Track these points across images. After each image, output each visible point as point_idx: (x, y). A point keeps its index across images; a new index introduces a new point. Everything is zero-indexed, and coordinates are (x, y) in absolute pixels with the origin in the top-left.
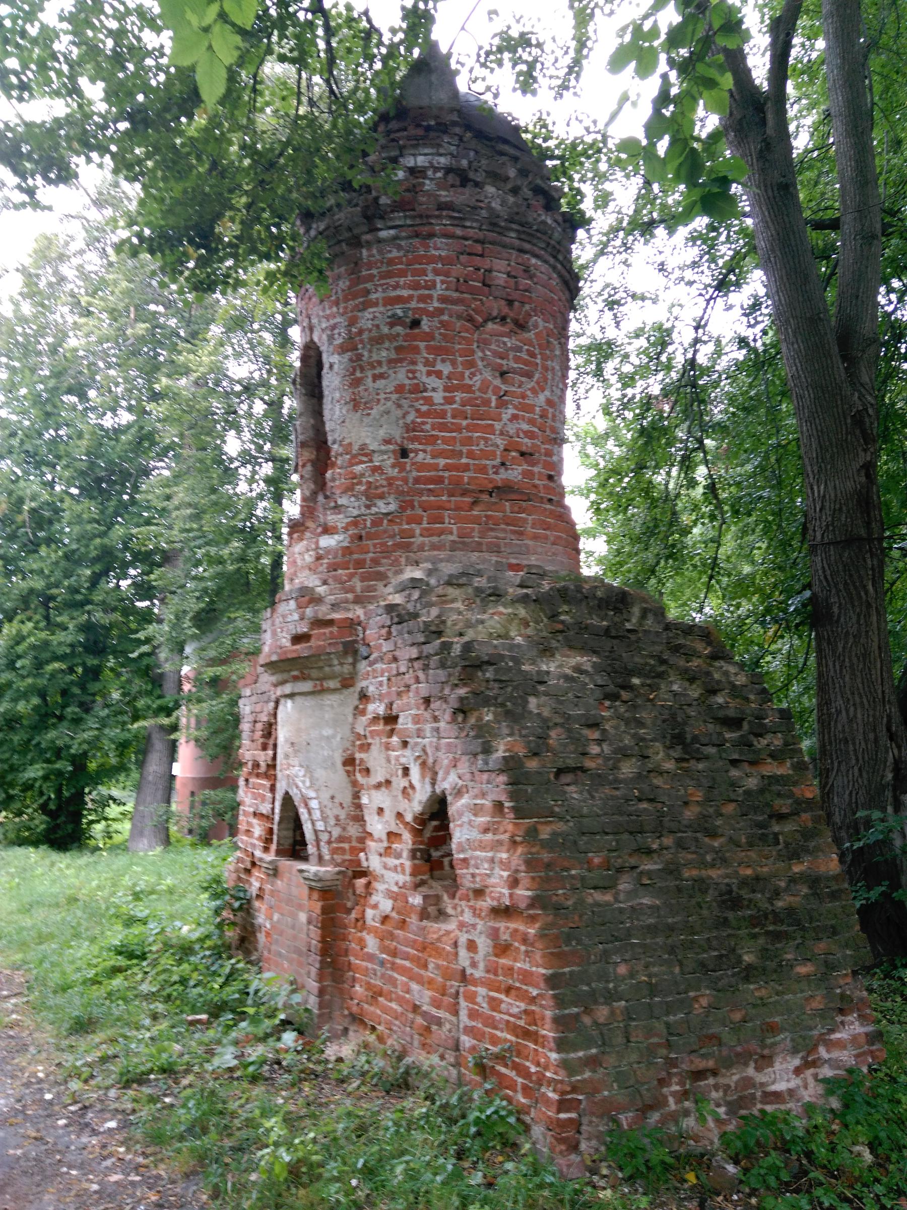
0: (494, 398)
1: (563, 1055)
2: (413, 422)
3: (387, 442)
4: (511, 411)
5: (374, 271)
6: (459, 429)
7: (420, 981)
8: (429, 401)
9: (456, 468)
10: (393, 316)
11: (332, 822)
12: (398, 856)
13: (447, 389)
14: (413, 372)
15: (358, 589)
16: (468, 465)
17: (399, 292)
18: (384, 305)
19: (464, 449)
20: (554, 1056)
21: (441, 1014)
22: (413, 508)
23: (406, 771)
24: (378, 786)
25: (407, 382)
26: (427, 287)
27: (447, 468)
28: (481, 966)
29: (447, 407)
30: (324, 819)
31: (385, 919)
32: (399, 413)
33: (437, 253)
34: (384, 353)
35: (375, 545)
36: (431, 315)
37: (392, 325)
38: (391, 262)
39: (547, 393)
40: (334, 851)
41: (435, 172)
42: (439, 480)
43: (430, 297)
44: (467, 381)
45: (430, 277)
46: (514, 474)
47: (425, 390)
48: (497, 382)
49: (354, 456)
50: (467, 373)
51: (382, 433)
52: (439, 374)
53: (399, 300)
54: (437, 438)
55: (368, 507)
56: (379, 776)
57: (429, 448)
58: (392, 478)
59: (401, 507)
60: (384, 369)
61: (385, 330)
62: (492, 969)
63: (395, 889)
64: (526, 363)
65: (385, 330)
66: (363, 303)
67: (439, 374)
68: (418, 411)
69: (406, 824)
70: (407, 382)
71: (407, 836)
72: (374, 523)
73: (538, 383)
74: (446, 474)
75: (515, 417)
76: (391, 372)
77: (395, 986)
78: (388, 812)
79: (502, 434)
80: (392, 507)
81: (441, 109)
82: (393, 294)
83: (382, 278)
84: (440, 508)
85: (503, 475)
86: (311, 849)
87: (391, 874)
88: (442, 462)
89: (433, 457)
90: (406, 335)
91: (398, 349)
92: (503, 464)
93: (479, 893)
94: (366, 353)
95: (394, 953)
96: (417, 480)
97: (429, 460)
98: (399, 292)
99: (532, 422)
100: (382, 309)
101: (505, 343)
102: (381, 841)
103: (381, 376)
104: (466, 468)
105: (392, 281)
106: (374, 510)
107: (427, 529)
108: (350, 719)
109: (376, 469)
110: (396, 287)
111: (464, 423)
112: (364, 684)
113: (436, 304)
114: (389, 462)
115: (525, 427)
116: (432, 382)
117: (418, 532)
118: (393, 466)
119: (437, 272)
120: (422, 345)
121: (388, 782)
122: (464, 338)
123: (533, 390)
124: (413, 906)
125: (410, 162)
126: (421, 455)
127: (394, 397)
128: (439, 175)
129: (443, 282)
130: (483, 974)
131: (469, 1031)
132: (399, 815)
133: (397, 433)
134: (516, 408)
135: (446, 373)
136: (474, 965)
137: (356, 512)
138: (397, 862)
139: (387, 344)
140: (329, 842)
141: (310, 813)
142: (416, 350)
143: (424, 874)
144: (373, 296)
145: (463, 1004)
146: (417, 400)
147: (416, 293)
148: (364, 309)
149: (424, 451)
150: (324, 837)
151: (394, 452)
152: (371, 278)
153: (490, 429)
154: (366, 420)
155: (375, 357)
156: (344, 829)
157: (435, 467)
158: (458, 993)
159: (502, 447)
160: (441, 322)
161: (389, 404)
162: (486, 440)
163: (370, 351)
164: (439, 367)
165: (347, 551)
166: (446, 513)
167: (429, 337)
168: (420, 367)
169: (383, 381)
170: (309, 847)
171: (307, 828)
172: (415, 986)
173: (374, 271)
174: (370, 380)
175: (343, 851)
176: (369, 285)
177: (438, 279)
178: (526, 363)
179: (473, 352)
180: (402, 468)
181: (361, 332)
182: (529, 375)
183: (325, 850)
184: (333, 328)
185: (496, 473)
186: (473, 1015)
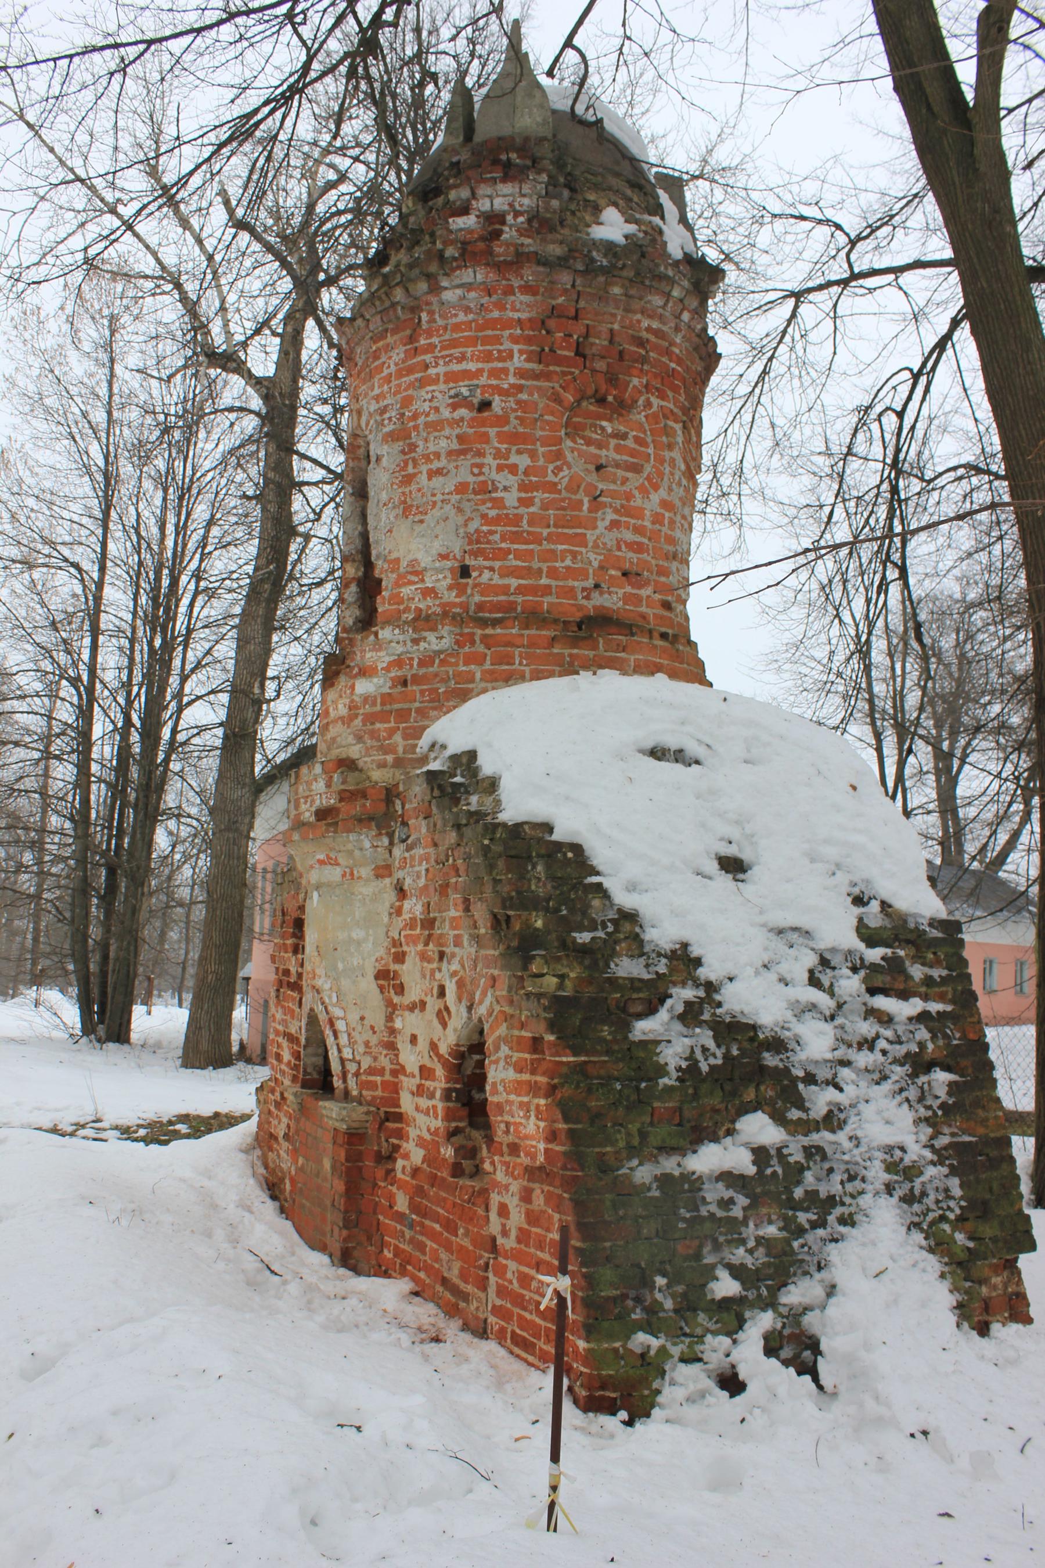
0: (586, 500)
1: (592, 1345)
2: (477, 531)
3: (444, 557)
4: (610, 516)
5: (435, 340)
6: (537, 540)
7: (448, 1247)
8: (499, 503)
9: (533, 590)
10: (456, 395)
11: (361, 1049)
12: (431, 1096)
13: (523, 487)
14: (480, 466)
15: (400, 749)
16: (549, 587)
17: (464, 366)
18: (445, 382)
19: (544, 567)
20: (582, 1344)
21: (469, 1288)
22: (473, 643)
23: (442, 993)
24: (412, 1008)
25: (471, 479)
26: (500, 359)
27: (521, 590)
28: (513, 1234)
29: (522, 510)
30: (352, 1043)
31: (416, 1171)
32: (460, 520)
33: (516, 315)
34: (443, 443)
35: (422, 692)
36: (504, 393)
37: (454, 407)
38: (457, 327)
39: (662, 493)
40: (363, 1085)
41: (515, 217)
42: (511, 607)
43: (505, 371)
44: (551, 477)
45: (507, 345)
46: (612, 600)
47: (496, 489)
48: (592, 478)
49: (401, 577)
50: (551, 467)
51: (437, 547)
52: (513, 469)
53: (467, 374)
54: (509, 551)
55: (416, 642)
56: (413, 994)
57: (497, 564)
58: (448, 604)
59: (457, 642)
60: (443, 463)
61: (446, 413)
62: (523, 1236)
63: (427, 1137)
64: (633, 453)
65: (446, 413)
66: (420, 380)
67: (513, 469)
68: (484, 516)
69: (440, 1056)
70: (471, 479)
71: (440, 1072)
72: (422, 663)
73: (648, 478)
74: (520, 599)
75: (614, 524)
76: (451, 466)
77: (424, 1253)
78: (425, 1040)
79: (596, 546)
80: (446, 643)
81: (527, 139)
82: (455, 367)
83: (443, 348)
84: (508, 644)
85: (598, 600)
86: (337, 1083)
87: (424, 1117)
88: (514, 583)
89: (501, 576)
90: (473, 419)
91: (461, 438)
92: (597, 586)
93: (514, 1149)
94: (421, 443)
95: (424, 1213)
96: (480, 607)
97: (497, 580)
98: (464, 366)
99: (638, 530)
100: (442, 387)
101: (603, 429)
102: (414, 1076)
103: (439, 472)
104: (547, 590)
105: (456, 352)
106: (423, 645)
107: (492, 672)
108: (386, 919)
109: (427, 592)
110: (462, 358)
111: (545, 532)
112: (400, 874)
113: (512, 380)
114: (445, 583)
115: (629, 536)
116: (505, 479)
117: (478, 676)
118: (450, 588)
119: (515, 340)
120: (492, 432)
121: (423, 1004)
122: (548, 423)
123: (642, 489)
124: (445, 1160)
125: (484, 205)
126: (487, 575)
127: (455, 498)
128: (521, 219)
129: (521, 352)
130: (515, 1245)
131: (497, 1311)
132: (434, 1046)
133: (457, 546)
134: (616, 511)
135: (521, 468)
136: (505, 1233)
137: (400, 649)
138: (430, 1103)
139: (447, 431)
140: (357, 1074)
141: (336, 1037)
142: (485, 438)
143: (460, 1120)
144: (432, 371)
145: (493, 1279)
146: (484, 502)
147: (487, 366)
148: (421, 387)
149: (492, 569)
150: (352, 1068)
151: (452, 570)
152: (430, 348)
153: (582, 541)
154: (418, 528)
155: (432, 448)
156: (375, 1059)
157: (505, 590)
158: (487, 1265)
159: (596, 564)
160: (518, 402)
161: (448, 507)
162: (574, 555)
163: (426, 440)
164: (514, 459)
165: (387, 698)
166: (517, 652)
167: (502, 420)
168: (489, 460)
169: (441, 479)
170: (335, 1079)
171: (333, 1054)
172: (444, 1255)
173: (435, 340)
174: (424, 477)
175: (372, 1086)
176: (428, 358)
177: (516, 348)
178: (633, 453)
179: (560, 441)
180: (461, 590)
181: (415, 416)
182: (636, 469)
183: (352, 1083)
184: (383, 411)
185: (587, 598)
186: (501, 1292)
